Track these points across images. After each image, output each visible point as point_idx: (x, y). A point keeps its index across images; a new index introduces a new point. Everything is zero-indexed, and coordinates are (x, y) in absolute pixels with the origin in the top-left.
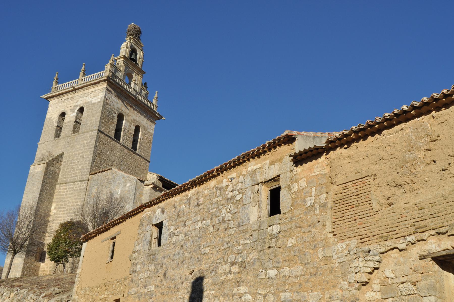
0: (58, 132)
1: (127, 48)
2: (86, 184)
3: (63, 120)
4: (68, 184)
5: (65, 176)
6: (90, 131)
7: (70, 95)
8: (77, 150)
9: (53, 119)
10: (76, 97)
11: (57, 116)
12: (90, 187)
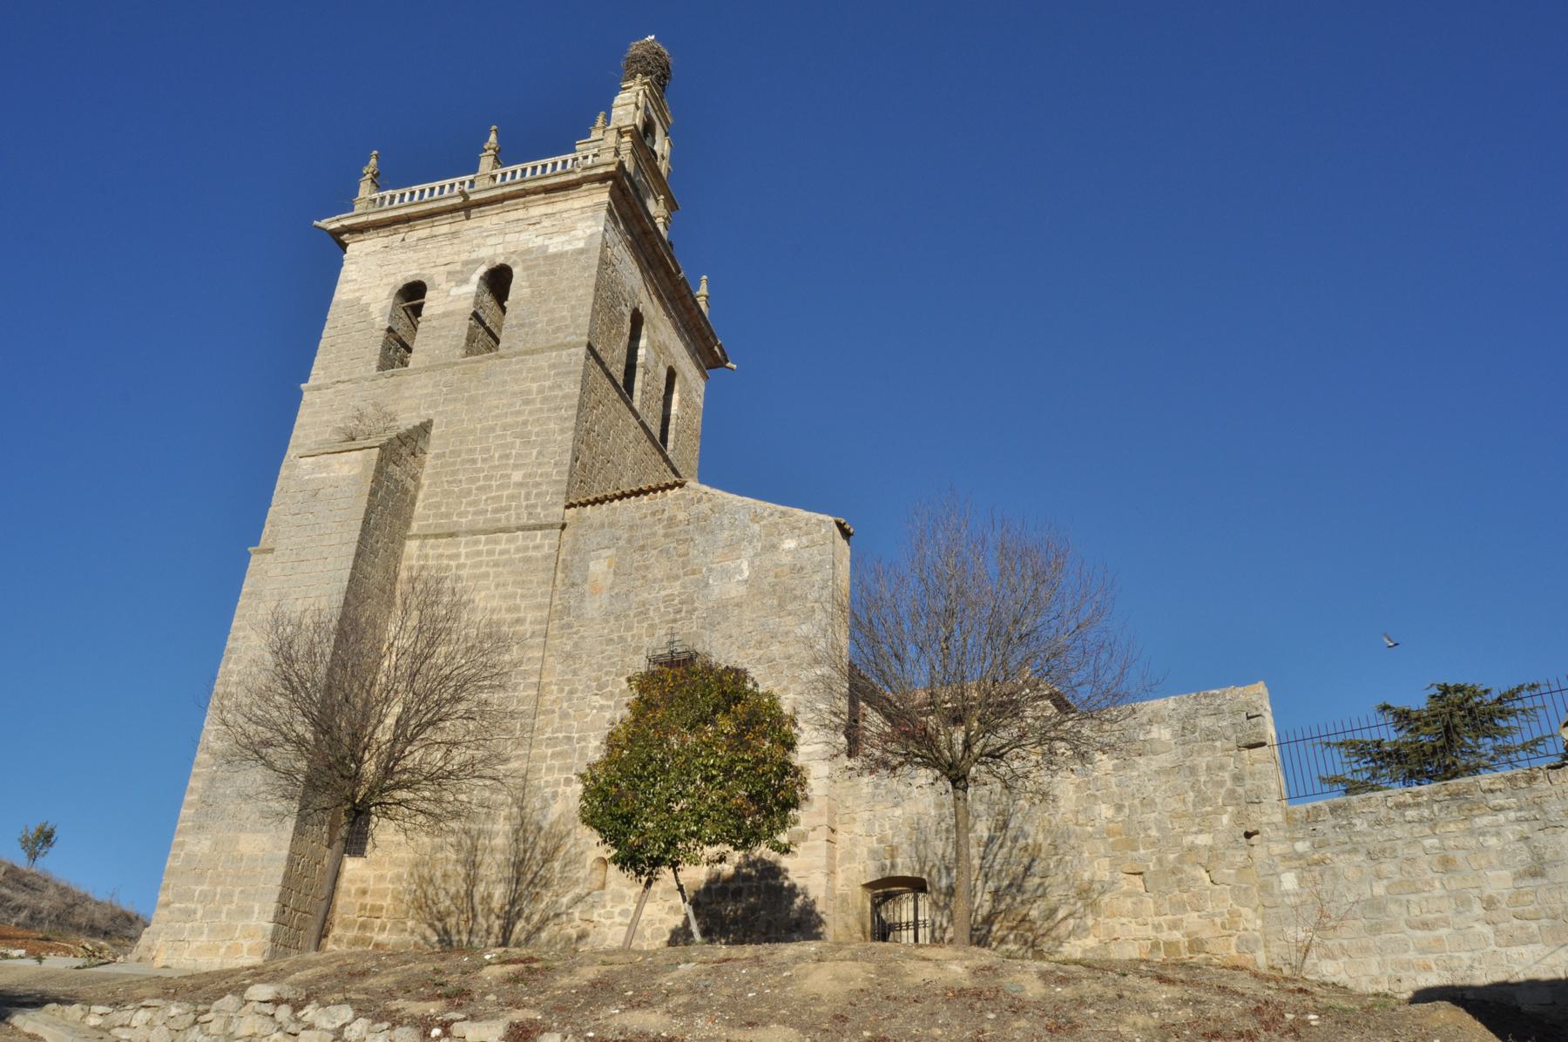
0: (391, 352)
1: (637, 107)
2: (555, 541)
3: (417, 311)
4: (463, 540)
5: (443, 510)
6: (552, 348)
7: (443, 227)
8: (494, 413)
9: (368, 304)
10: (470, 232)
11: (387, 293)
12: (574, 551)
